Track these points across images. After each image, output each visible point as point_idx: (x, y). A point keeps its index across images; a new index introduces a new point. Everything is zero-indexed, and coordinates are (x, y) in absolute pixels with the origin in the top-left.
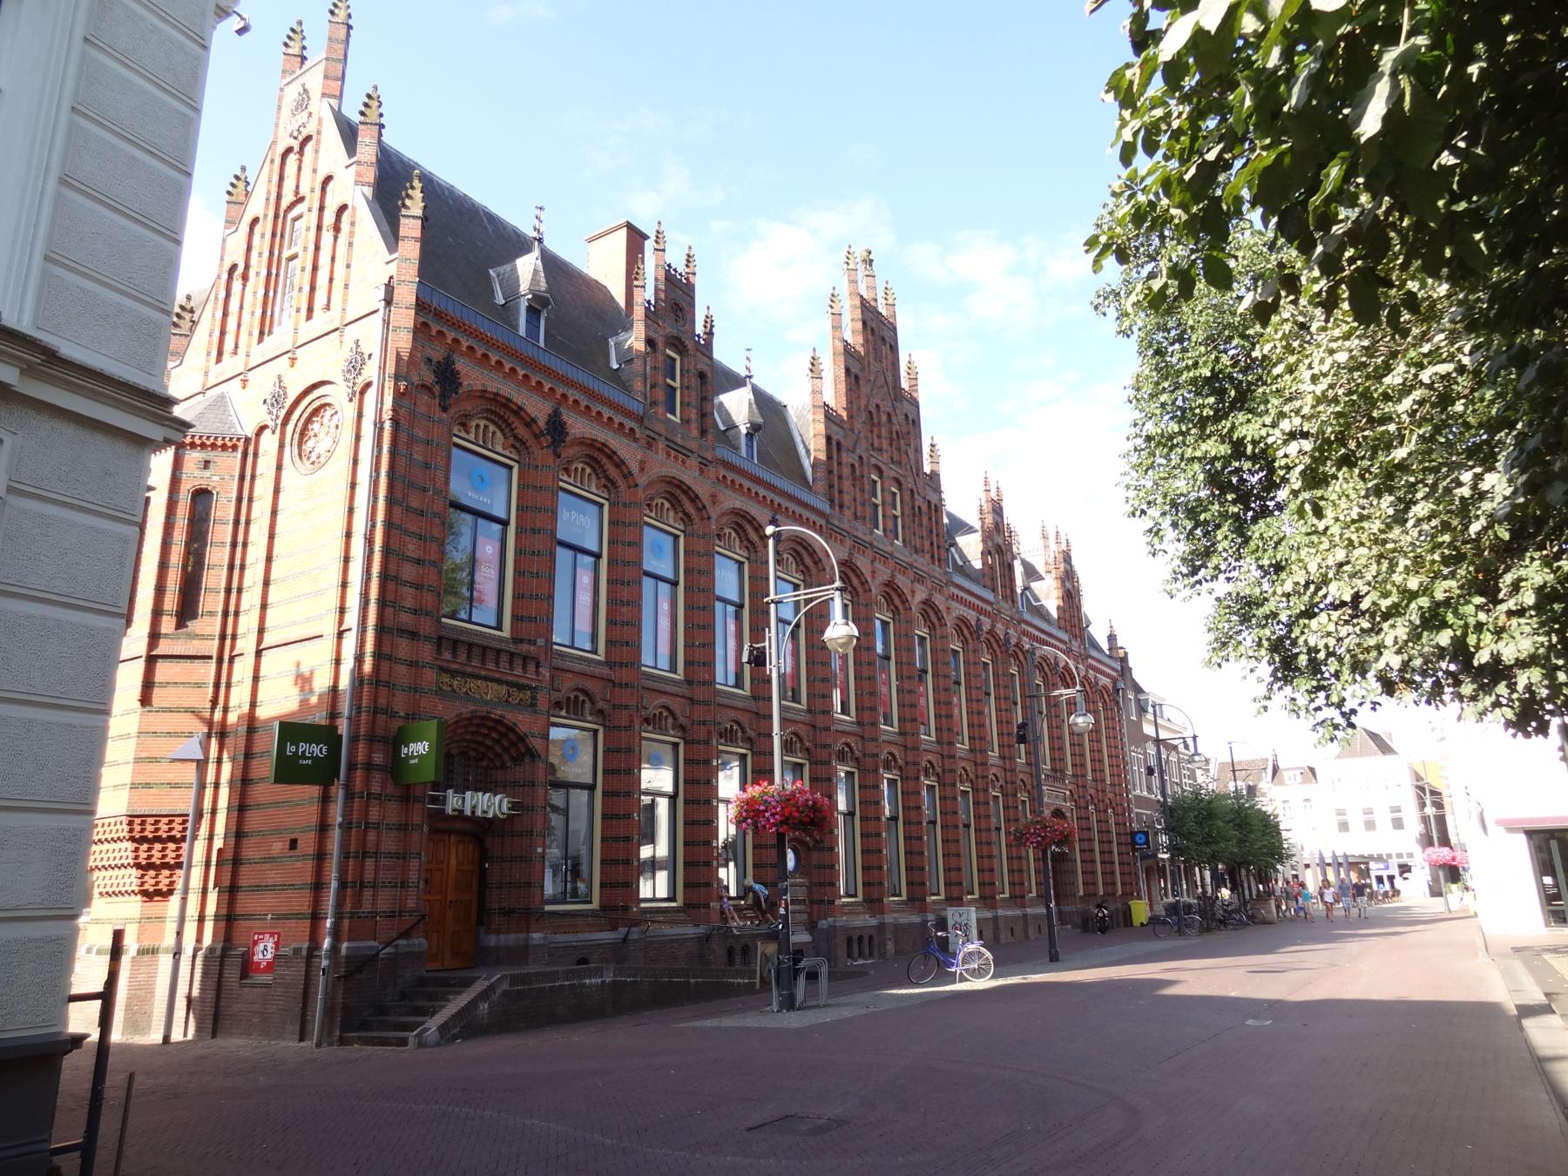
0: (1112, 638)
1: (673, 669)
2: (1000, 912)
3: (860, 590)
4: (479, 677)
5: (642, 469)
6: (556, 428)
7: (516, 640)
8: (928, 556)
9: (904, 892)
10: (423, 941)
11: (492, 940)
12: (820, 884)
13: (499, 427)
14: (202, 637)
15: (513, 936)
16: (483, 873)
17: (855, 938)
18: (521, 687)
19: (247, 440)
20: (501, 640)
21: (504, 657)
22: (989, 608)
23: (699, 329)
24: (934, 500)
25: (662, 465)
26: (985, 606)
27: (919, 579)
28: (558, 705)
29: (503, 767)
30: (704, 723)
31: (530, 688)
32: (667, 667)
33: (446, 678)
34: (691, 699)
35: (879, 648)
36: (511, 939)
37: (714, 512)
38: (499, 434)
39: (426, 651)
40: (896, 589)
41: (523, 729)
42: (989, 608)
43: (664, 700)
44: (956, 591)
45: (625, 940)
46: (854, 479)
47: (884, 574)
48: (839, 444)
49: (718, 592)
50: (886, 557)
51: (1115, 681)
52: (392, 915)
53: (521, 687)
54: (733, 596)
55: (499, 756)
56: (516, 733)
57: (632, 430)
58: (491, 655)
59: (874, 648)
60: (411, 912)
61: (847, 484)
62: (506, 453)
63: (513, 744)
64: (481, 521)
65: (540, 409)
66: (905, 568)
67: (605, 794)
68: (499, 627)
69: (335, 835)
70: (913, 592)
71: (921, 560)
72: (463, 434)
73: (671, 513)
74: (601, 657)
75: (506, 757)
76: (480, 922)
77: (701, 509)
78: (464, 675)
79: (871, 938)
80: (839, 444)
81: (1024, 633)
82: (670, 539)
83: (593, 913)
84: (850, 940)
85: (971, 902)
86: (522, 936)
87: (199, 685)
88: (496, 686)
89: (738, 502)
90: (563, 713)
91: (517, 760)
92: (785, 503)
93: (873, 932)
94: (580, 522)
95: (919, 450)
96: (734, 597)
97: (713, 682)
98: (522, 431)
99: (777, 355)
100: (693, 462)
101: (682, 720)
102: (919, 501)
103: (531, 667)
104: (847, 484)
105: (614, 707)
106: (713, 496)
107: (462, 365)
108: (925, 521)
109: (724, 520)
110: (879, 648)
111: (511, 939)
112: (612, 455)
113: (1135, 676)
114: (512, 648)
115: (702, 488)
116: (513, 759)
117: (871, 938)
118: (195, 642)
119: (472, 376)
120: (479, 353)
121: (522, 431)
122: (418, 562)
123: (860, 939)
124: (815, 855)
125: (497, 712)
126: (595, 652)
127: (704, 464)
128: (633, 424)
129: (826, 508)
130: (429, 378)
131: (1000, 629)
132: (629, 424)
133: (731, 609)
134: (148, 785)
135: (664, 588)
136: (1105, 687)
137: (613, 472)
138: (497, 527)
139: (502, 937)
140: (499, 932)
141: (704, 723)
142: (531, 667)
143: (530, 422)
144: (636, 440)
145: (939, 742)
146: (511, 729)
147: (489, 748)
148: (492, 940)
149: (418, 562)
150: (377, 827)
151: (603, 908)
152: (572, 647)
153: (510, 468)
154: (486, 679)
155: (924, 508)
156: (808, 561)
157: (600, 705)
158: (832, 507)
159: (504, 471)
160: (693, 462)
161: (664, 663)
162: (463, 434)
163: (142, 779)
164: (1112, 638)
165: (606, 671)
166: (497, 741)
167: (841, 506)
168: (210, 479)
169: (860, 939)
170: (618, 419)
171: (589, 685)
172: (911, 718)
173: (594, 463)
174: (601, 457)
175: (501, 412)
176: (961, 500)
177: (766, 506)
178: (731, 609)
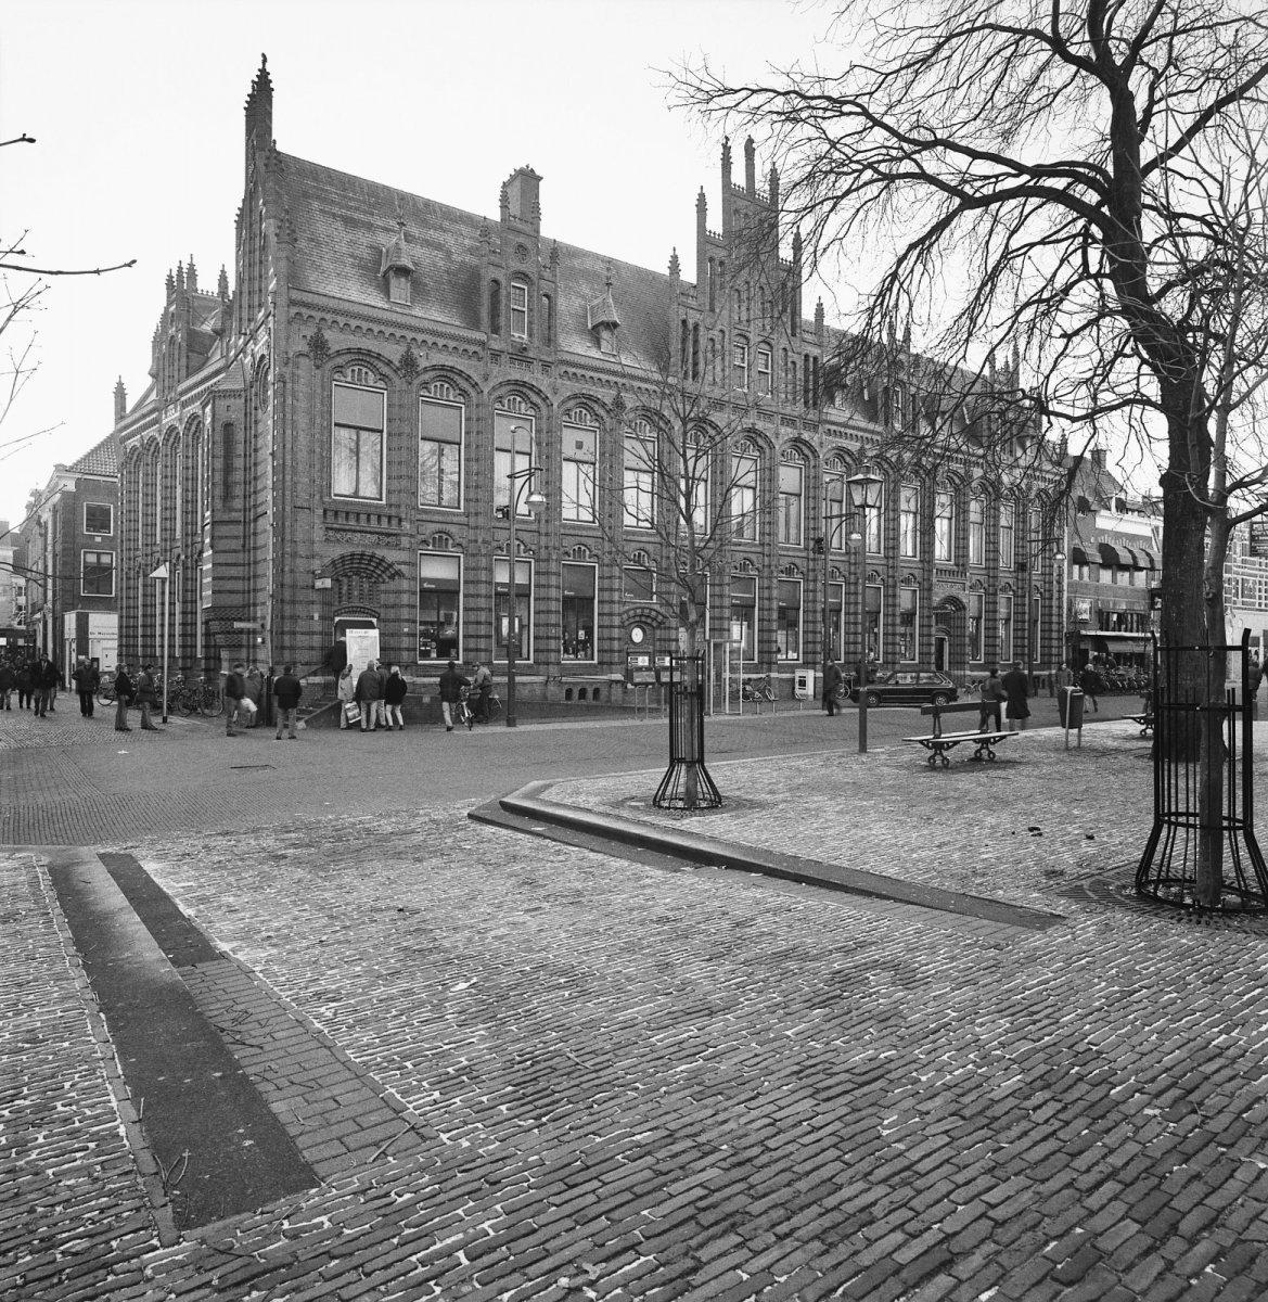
2: (774, 675)
4: (355, 531)
6: (409, 363)
7: (390, 505)
20: (381, 506)
21: (363, 517)
27: (788, 421)
33: (331, 533)
43: (642, 545)
47: (788, 432)
52: (306, 664)
62: (378, 385)
65: (394, 352)
67: (535, 599)
69: (158, 633)
73: (452, 391)
74: (384, 502)
77: (814, 452)
78: (345, 530)
89: (577, 387)
90: (430, 547)
91: (392, 577)
98: (385, 370)
100: (537, 366)
101: (802, 569)
102: (792, 356)
103: (395, 522)
107: (328, 335)
119: (335, 340)
120: (440, 345)
121: (385, 370)
124: (658, 632)
125: (369, 552)
127: (546, 366)
130: (306, 349)
132: (472, 348)
135: (703, 484)
142: (395, 522)
143: (389, 363)
144: (480, 359)
151: (599, 663)
155: (800, 363)
156: (806, 451)
160: (537, 366)
165: (463, 519)
170: (376, 328)
171: (583, 540)
174: (525, 390)
175: (364, 358)
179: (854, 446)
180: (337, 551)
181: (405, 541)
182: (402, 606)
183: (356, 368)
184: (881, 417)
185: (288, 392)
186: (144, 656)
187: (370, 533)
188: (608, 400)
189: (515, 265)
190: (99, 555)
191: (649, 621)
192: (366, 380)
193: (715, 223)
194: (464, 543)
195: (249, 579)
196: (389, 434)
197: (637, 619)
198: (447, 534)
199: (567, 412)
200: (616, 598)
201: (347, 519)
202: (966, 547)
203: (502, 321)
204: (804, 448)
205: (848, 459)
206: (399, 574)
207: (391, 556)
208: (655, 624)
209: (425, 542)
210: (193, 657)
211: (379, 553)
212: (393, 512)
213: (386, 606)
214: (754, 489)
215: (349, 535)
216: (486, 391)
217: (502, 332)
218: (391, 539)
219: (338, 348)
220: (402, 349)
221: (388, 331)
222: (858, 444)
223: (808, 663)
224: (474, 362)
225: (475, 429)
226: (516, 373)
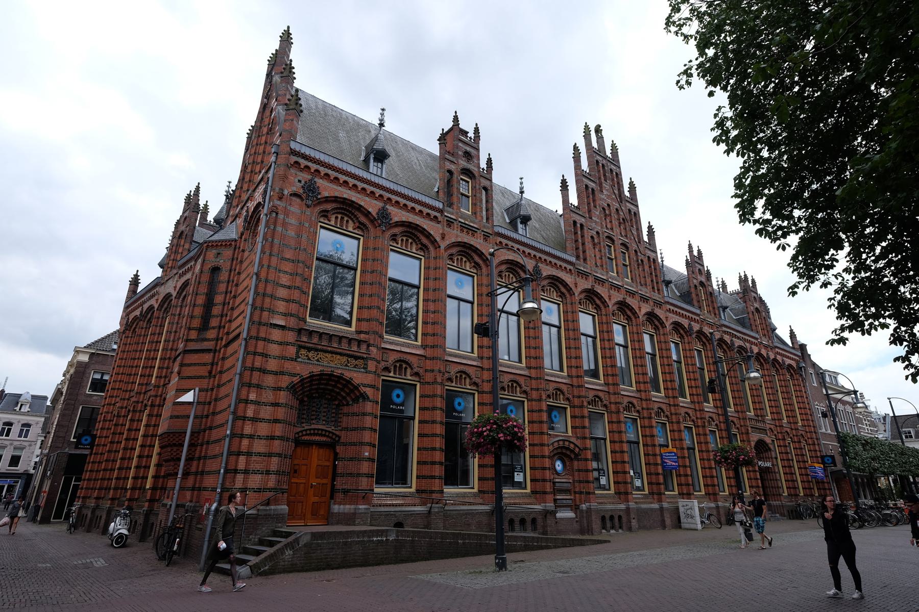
0: (793, 335)
1: (561, 370)
3: (602, 306)
5: (443, 238)
6: (384, 215)
7: (359, 332)
8: (650, 288)
9: (476, 486)
10: (286, 507)
11: (336, 508)
12: (580, 482)
13: (350, 217)
14: (208, 340)
15: (348, 506)
16: (335, 466)
17: (607, 517)
18: (356, 358)
19: (236, 241)
22: (697, 318)
23: (483, 165)
24: (652, 255)
25: (456, 235)
26: (694, 317)
27: (645, 299)
28: (387, 369)
29: (348, 405)
30: (433, 371)
31: (363, 358)
32: (517, 360)
33: (303, 352)
34: (572, 385)
35: (674, 357)
36: (347, 508)
37: (667, 324)
38: (350, 222)
39: (291, 337)
40: (656, 317)
41: (356, 381)
42: (697, 318)
44: (672, 308)
45: (430, 512)
46: (594, 245)
48: (582, 225)
49: (582, 330)
50: (618, 288)
51: (797, 362)
52: (259, 490)
53: (356, 358)
54: (622, 342)
55: (344, 398)
56: (352, 385)
57: (435, 217)
58: (344, 341)
59: (671, 357)
60: (270, 490)
61: (589, 245)
62: (356, 231)
63: (352, 391)
64: (461, 303)
65: (373, 206)
66: (632, 294)
67: (420, 422)
68: (472, 352)
70: (640, 308)
71: (644, 289)
72: (326, 222)
73: (468, 264)
75: (348, 399)
76: (332, 497)
78: (316, 350)
79: (620, 517)
80: (582, 225)
81: (725, 332)
82: (591, 317)
83: (411, 495)
84: (603, 518)
85: (696, 497)
86: (353, 507)
87: (205, 364)
88: (338, 357)
89: (511, 256)
90: (392, 374)
91: (356, 400)
92: (544, 257)
93: (621, 513)
94: (551, 313)
95: (639, 229)
96: (591, 333)
97: (443, 347)
99: (537, 178)
101: (475, 380)
102: (641, 257)
104: (589, 245)
105: (426, 371)
106: (576, 284)
108: (647, 268)
109: (503, 267)
110: (674, 357)
111: (347, 508)
112: (423, 231)
113: (813, 358)
114: (355, 337)
115: (568, 279)
116: (353, 400)
117: (620, 517)
118: (205, 343)
121: (363, 219)
122: (289, 287)
123: (612, 518)
124: (576, 463)
125: (338, 372)
126: (472, 352)
127: (486, 237)
128: (438, 215)
129: (573, 259)
131: (764, 352)
132: (569, 267)
133: (554, 330)
134: (177, 417)
136: (790, 366)
137: (424, 240)
138: (469, 305)
139: (342, 507)
140: (340, 504)
141: (433, 371)
143: (367, 214)
144: (439, 222)
145: (667, 397)
146: (349, 382)
147: (338, 393)
148: (336, 508)
149: (289, 287)
150: (251, 437)
151: (418, 491)
152: (459, 349)
153: (473, 277)
154: (332, 352)
155: (646, 260)
157: (605, 402)
158: (578, 257)
159: (471, 279)
161: (514, 356)
162: (326, 222)
163: (176, 413)
164: (793, 335)
166: (342, 390)
167: (585, 260)
168: (221, 262)
169: (612, 518)
171: (408, 357)
172: (792, 417)
173: (552, 285)
176: (674, 260)
177: (531, 258)
178: (590, 340)
179: (685, 322)
180: (304, 368)
181: (371, 366)
182: (364, 429)
183: (339, 216)
184: (696, 303)
185: (280, 222)
186: (133, 488)
187: (341, 354)
188: (373, 211)
189: (463, 163)
190: (103, 374)
191: (568, 453)
192: (347, 227)
193: (585, 165)
194: (421, 371)
195: (210, 403)
196: (363, 272)
197: (559, 451)
198: (407, 363)
199: (451, 257)
200: (250, 413)
201: (340, 343)
202: (539, 347)
203: (455, 200)
204: (560, 286)
205: (681, 331)
206: (364, 397)
207: (358, 377)
208: (573, 456)
209: (387, 369)
210: (142, 489)
211: (348, 375)
212: (362, 336)
213: (346, 429)
214: (472, 303)
215: (321, 355)
216: (442, 247)
217: (455, 207)
218: (360, 362)
219: (326, 194)
220: (380, 204)
221: (343, 178)
222: (380, 204)
223: (683, 494)
224: (568, 275)
225: (432, 277)
226: (466, 238)
